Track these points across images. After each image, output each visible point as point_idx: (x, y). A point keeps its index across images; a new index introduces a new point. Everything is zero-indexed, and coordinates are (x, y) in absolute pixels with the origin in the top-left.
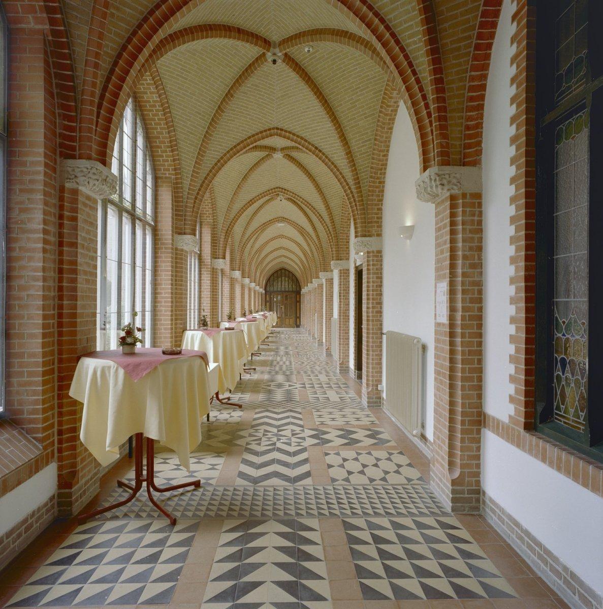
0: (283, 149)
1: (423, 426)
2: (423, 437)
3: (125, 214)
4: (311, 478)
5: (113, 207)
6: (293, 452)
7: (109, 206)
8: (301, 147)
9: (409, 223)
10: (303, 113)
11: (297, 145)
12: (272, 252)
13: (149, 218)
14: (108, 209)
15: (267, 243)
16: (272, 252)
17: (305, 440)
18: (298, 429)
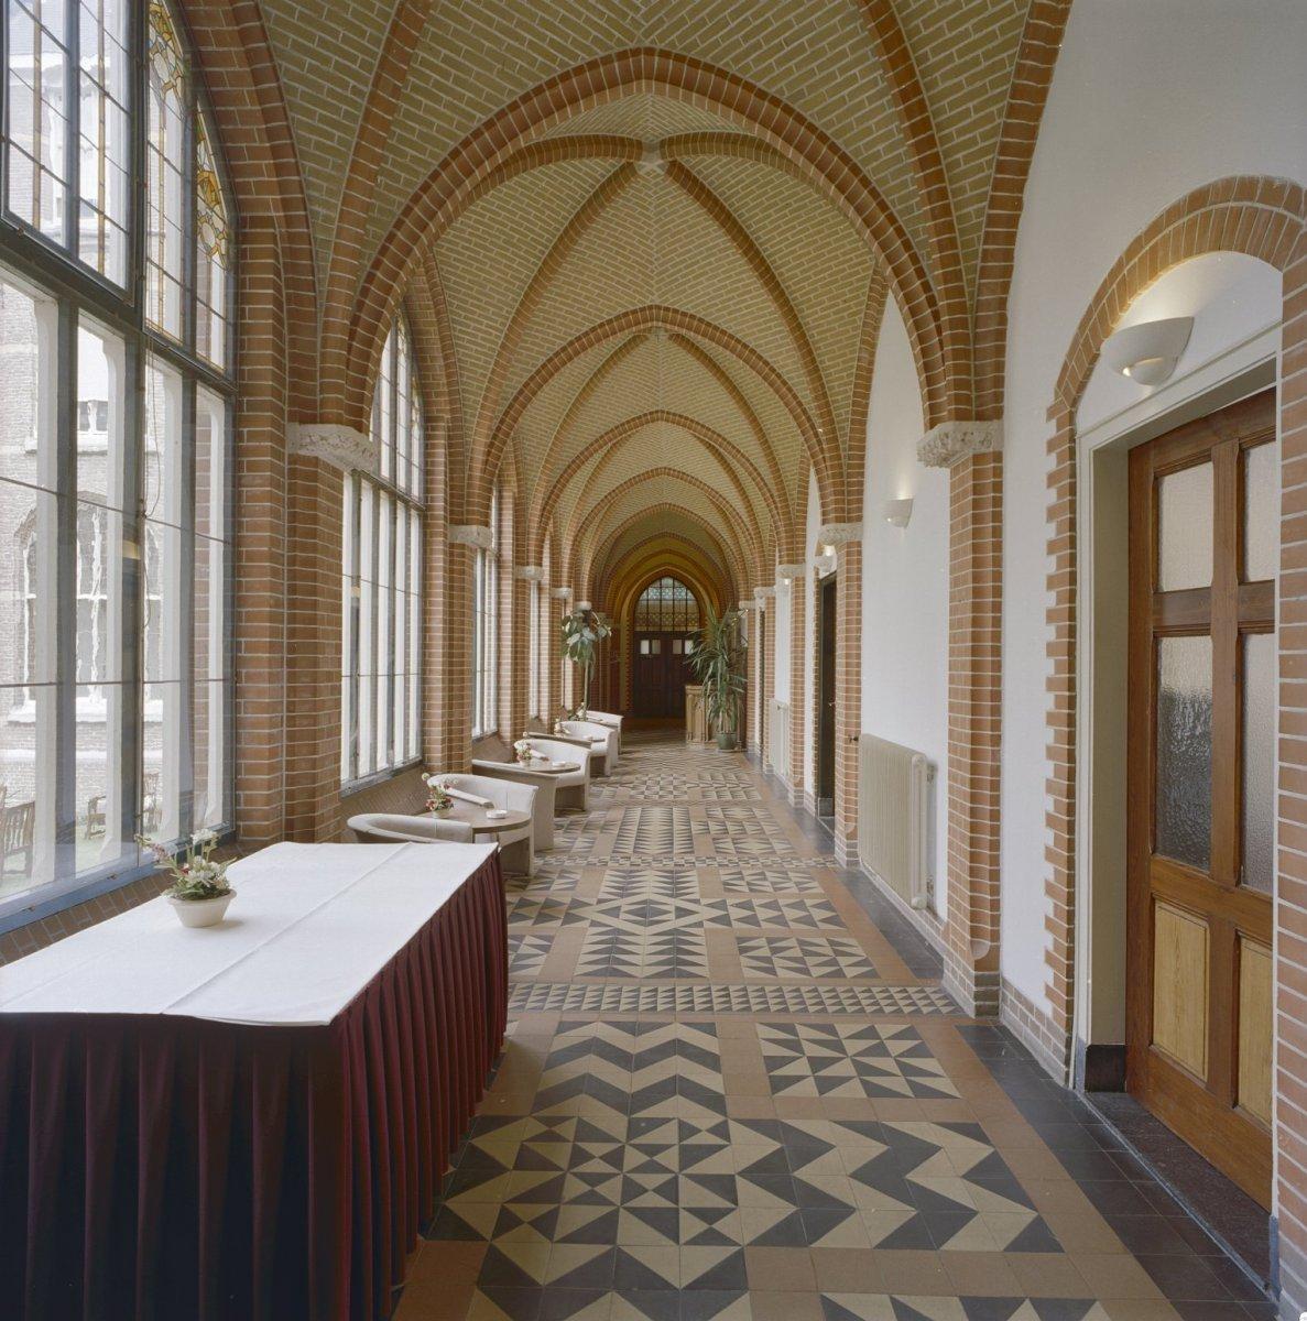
0: (668, 144)
1: (930, 887)
2: (931, 908)
3: (383, 494)
4: (746, 1298)
5: (159, 362)
6: (673, 1093)
7: (81, 319)
8: (779, 144)
9: (902, 496)
10: (722, 290)
11: (768, 136)
12: (636, 548)
13: (416, 491)
14: (81, 331)
15: (629, 554)
16: (636, 548)
17: (727, 1137)
18: (704, 1118)
